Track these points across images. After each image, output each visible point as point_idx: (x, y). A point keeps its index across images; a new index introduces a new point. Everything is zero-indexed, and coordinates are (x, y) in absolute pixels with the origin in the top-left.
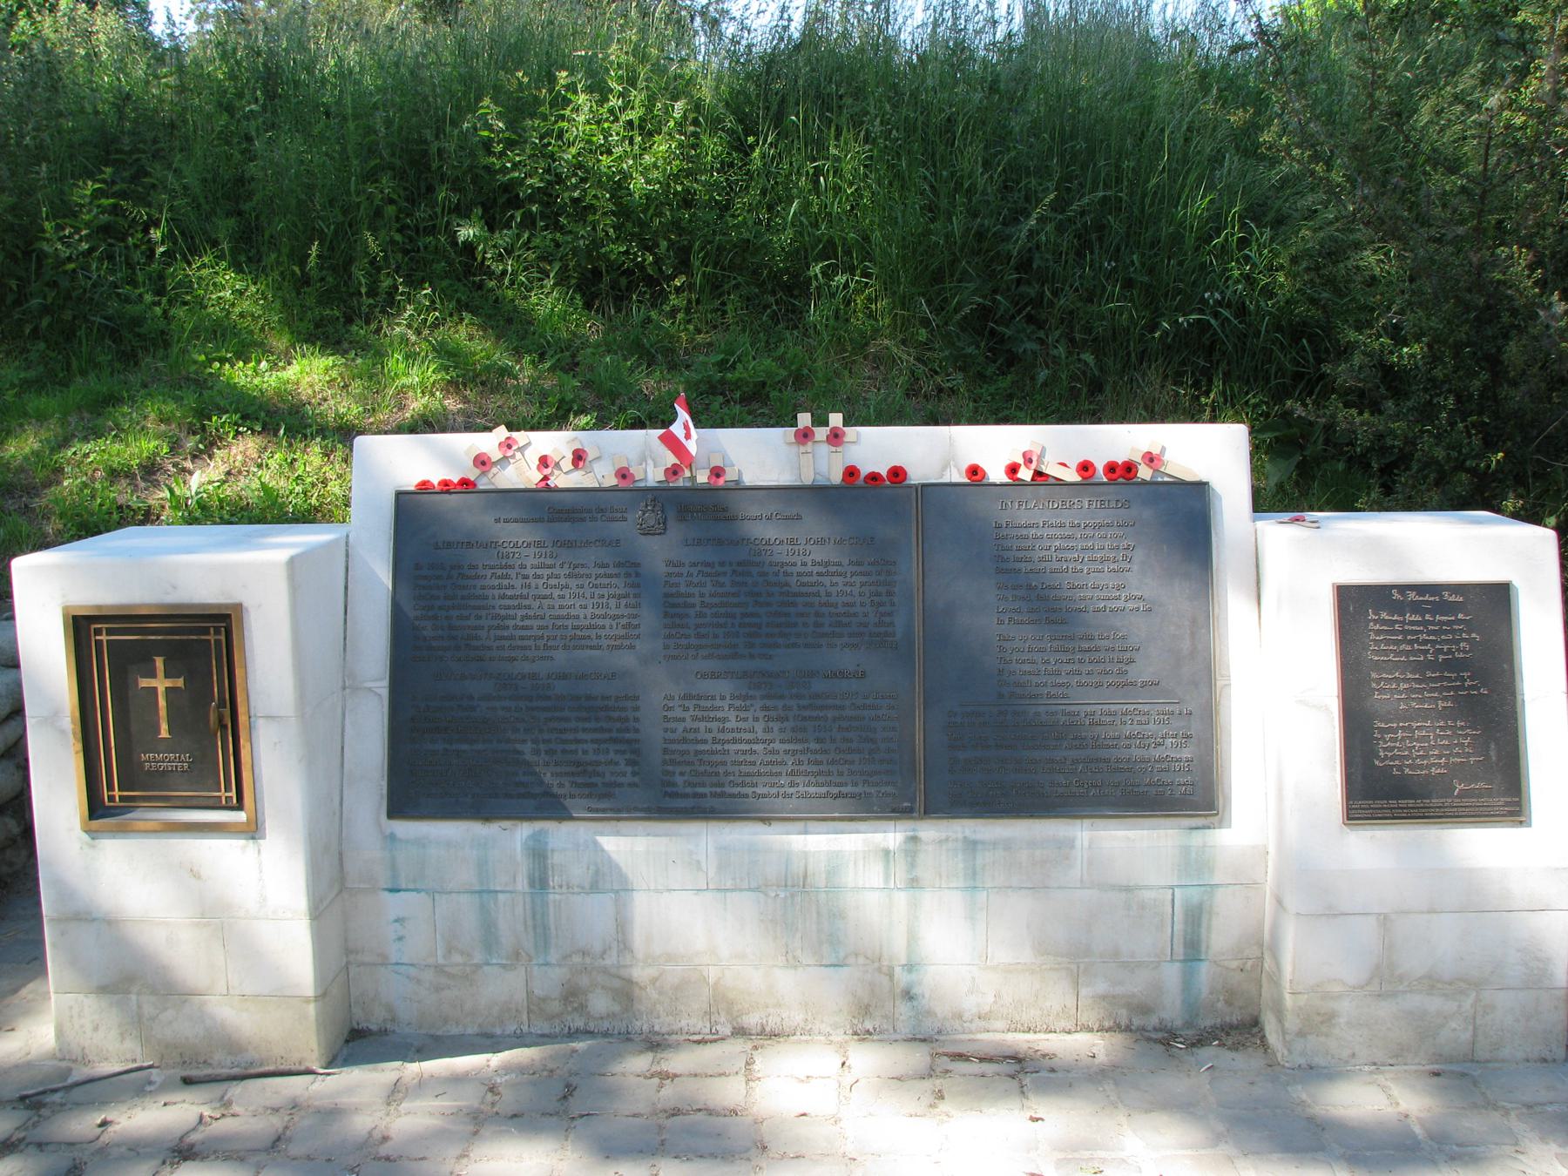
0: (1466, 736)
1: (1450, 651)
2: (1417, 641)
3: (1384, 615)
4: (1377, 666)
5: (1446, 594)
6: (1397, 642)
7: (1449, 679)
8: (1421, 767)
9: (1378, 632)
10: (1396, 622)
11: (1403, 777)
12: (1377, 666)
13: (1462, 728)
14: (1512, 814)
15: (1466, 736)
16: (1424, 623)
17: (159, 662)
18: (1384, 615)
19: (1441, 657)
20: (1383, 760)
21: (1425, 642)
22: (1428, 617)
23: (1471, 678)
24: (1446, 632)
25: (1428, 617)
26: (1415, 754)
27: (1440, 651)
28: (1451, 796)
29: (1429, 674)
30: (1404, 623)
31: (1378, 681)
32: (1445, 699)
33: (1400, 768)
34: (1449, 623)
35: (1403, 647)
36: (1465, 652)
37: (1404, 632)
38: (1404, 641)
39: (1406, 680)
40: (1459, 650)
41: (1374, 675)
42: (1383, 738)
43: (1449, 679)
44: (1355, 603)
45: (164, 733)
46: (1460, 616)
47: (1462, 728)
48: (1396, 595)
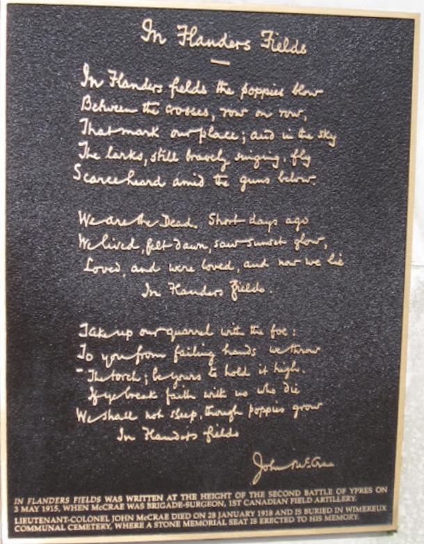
0: (287, 358)
1: (266, 168)
2: (192, 142)
3: (118, 80)
4: (99, 201)
5: (268, 34)
6: (147, 146)
7: (260, 233)
8: (182, 426)
9: (99, 120)
10: (146, 95)
11: (141, 444)
12: (99, 201)
13: (281, 342)
14: (366, 519)
15: (287, 358)
16: (212, 101)
17: (240, 414)
18: (118, 80)
19: (245, 180)
20: (93, 411)
21: (211, 146)
22: (221, 87)
23: (310, 231)
24: (260, 124)
25: (221, 87)
26: (170, 397)
27: (247, 168)
28: (246, 487)
29: (214, 219)
30: (164, 97)
31: (94, 234)
32: (247, 276)
33: (131, 428)
34: (265, 102)
35: (160, 155)
36: (300, 169)
37: (168, 121)
38: (165, 142)
39: (159, 233)
40: (287, 167)
41: (85, 219)
42: (98, 364)
43: (260, 233)
44: (410, 23)
46: (298, 90)
47: (281, 342)
48: (151, 33)
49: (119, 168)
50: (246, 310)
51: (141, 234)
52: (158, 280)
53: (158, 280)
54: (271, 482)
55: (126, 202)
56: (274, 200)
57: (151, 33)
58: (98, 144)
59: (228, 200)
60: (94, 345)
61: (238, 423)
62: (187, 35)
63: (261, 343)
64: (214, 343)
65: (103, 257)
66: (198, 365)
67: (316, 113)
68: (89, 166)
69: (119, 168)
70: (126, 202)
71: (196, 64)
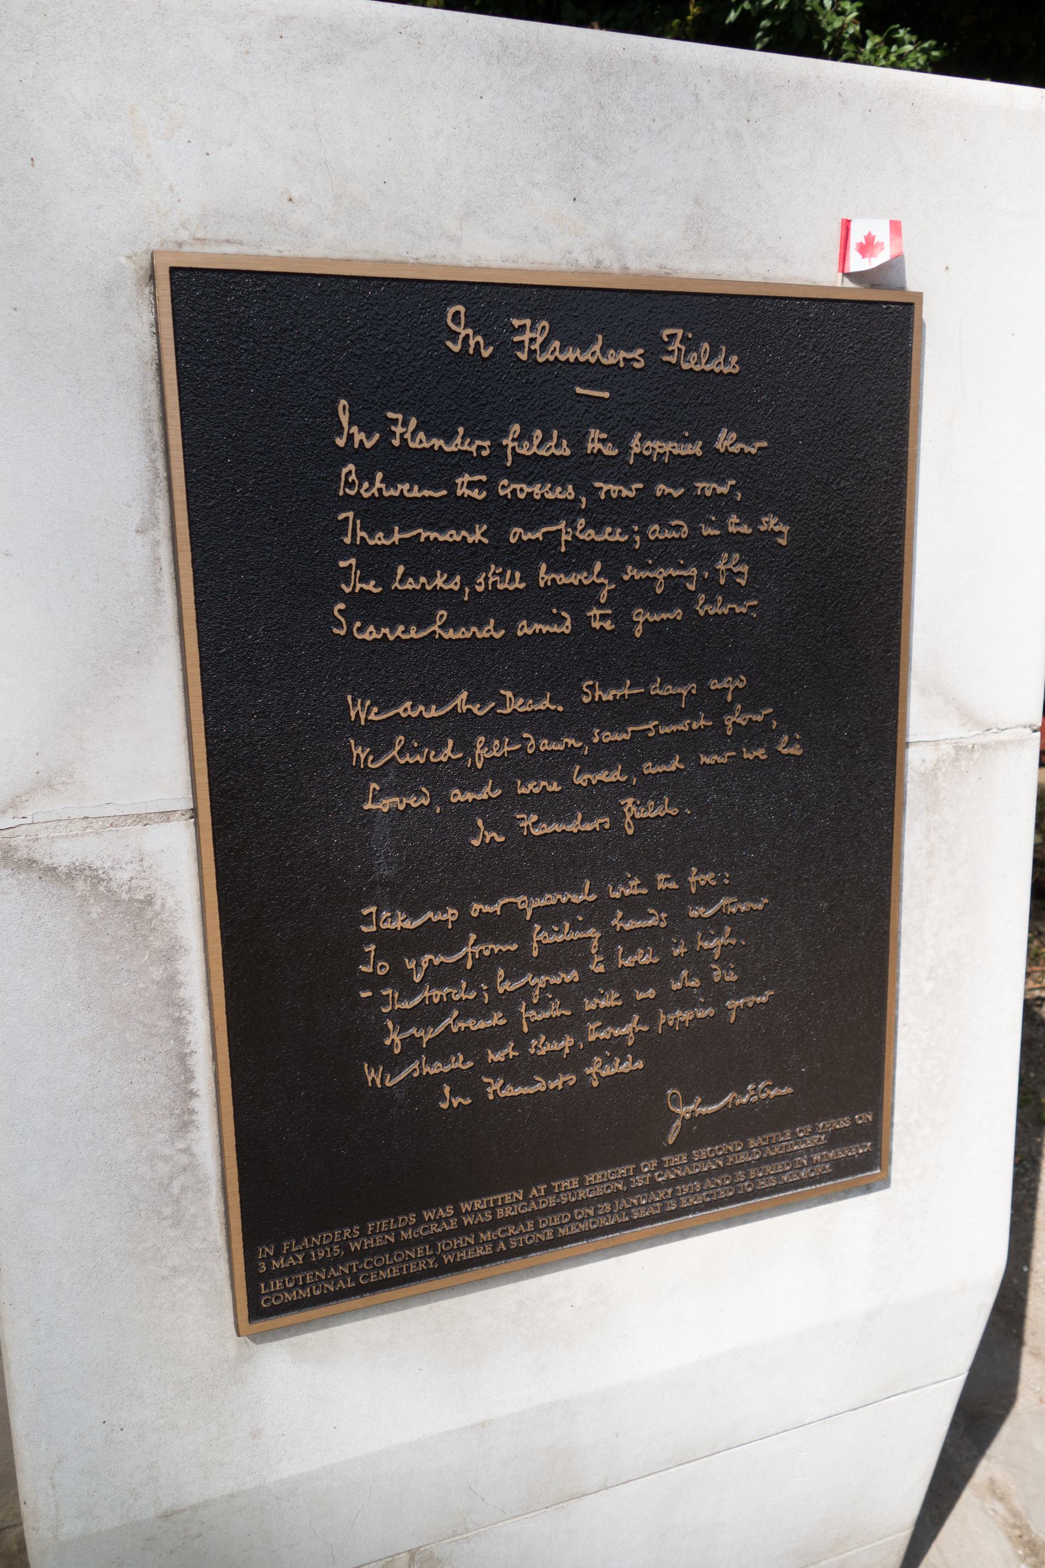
2: (465, 561)
3: (408, 432)
6: (465, 561)
9: (378, 513)
18: (408, 432)
32: (647, 789)
37: (500, 513)
39: (498, 726)
48: (465, 336)
49: (417, 608)
50: (647, 850)
51: (463, 728)
52: (498, 814)
53: (498, 814)
57: (465, 336)
58: (376, 563)
60: (394, 945)
61: (643, 1045)
63: (674, 903)
64: (597, 913)
65: (403, 780)
66: (572, 955)
68: (363, 608)
69: (417, 608)
71: (542, 393)
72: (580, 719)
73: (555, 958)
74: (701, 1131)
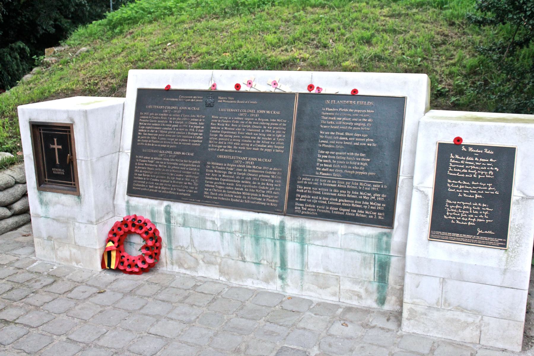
3: (457, 157)
6: (461, 169)
9: (453, 164)
16: (475, 161)
18: (457, 157)
45: (58, 162)
49: (456, 172)
52: (462, 193)
53: (462, 193)
54: (481, 235)
55: (457, 178)
56: (485, 180)
59: (476, 180)
62: (470, 149)
64: (472, 206)
65: (452, 188)
66: (468, 210)
67: (494, 165)
69: (456, 172)
70: (457, 178)
71: (472, 155)
72: (472, 185)
73: (468, 210)
74: (481, 235)
